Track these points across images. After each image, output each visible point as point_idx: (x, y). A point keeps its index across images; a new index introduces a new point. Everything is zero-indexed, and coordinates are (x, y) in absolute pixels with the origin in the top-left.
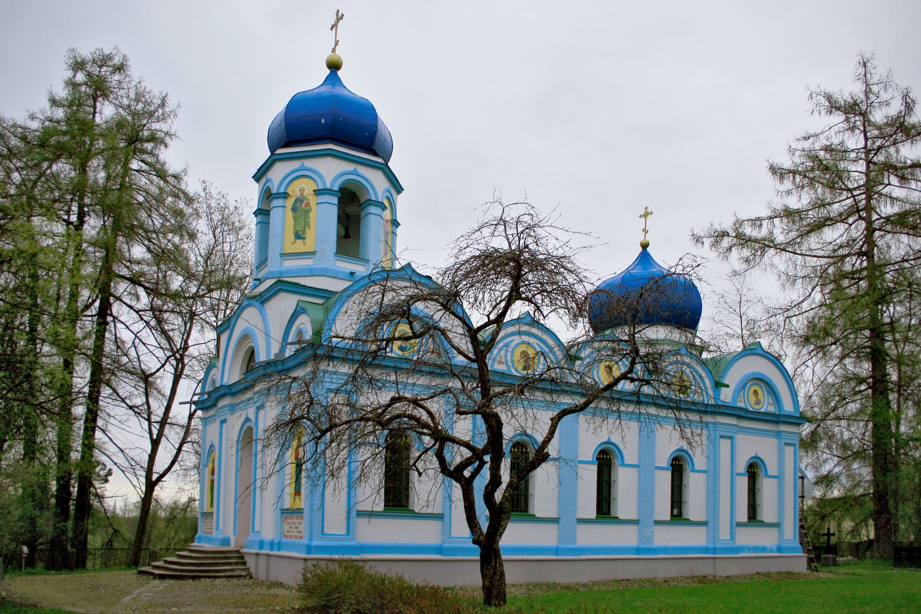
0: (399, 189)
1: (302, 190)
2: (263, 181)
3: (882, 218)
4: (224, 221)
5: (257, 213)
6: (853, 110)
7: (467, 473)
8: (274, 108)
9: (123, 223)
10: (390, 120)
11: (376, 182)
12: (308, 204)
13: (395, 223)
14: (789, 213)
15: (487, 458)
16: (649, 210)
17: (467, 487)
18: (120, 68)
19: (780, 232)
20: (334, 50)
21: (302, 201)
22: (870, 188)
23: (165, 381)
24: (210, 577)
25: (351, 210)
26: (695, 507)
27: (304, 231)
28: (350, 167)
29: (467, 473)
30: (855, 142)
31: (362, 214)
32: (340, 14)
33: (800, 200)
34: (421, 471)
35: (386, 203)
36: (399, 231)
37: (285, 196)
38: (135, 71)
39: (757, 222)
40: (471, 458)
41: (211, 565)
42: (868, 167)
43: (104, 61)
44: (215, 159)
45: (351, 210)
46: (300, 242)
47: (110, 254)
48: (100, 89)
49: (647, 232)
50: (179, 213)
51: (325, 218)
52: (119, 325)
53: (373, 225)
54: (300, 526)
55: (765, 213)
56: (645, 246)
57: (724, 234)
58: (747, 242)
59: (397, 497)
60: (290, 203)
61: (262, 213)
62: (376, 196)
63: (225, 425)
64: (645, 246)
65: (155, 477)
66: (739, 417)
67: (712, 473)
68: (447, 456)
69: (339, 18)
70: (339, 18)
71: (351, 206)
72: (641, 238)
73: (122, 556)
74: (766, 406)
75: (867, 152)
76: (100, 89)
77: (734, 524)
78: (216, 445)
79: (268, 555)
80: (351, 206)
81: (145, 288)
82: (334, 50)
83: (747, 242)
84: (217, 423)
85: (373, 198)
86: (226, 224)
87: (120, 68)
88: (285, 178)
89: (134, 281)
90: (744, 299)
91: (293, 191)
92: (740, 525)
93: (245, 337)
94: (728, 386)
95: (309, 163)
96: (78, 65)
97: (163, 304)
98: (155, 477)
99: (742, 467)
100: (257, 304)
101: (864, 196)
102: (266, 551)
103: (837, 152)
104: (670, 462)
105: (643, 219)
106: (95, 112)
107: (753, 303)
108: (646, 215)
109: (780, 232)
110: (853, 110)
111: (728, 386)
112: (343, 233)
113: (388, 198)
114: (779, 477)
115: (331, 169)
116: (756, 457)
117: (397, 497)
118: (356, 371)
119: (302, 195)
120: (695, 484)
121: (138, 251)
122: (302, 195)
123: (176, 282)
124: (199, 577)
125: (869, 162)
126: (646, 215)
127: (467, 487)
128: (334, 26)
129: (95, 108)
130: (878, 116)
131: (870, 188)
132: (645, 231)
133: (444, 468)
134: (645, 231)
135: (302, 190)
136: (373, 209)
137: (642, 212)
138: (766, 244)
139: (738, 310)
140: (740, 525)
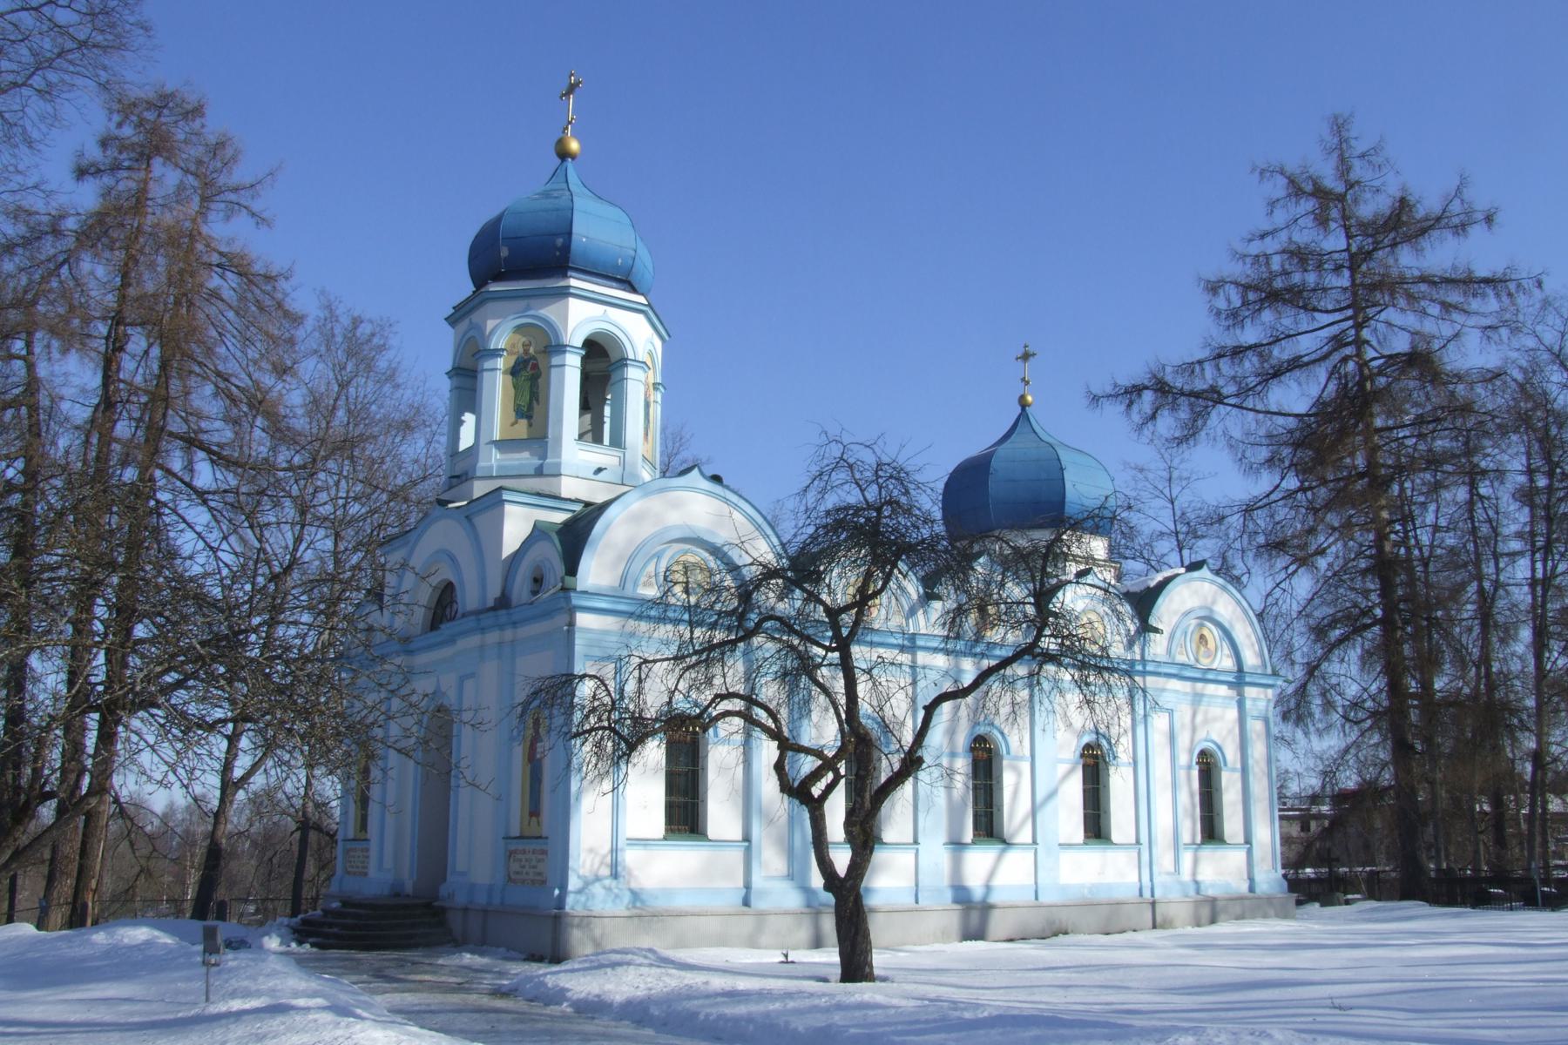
2: (464, 325)
6: (1327, 202)
7: (816, 791)
16: (1030, 350)
17: (816, 807)
18: (197, 111)
28: (599, 309)
29: (816, 791)
31: (614, 377)
38: (214, 125)
39: (1190, 368)
40: (819, 767)
45: (597, 366)
47: (160, 398)
55: (1205, 354)
56: (1023, 404)
57: (1135, 391)
58: (1177, 398)
59: (685, 815)
73: (188, 907)
83: (1177, 398)
87: (197, 111)
90: (1175, 474)
101: (1350, 323)
103: (1300, 256)
104: (1080, 750)
109: (1224, 376)
110: (1327, 202)
118: (132, 324)
120: (1119, 783)
124: (619, 964)
126: (1026, 357)
139: (1166, 491)
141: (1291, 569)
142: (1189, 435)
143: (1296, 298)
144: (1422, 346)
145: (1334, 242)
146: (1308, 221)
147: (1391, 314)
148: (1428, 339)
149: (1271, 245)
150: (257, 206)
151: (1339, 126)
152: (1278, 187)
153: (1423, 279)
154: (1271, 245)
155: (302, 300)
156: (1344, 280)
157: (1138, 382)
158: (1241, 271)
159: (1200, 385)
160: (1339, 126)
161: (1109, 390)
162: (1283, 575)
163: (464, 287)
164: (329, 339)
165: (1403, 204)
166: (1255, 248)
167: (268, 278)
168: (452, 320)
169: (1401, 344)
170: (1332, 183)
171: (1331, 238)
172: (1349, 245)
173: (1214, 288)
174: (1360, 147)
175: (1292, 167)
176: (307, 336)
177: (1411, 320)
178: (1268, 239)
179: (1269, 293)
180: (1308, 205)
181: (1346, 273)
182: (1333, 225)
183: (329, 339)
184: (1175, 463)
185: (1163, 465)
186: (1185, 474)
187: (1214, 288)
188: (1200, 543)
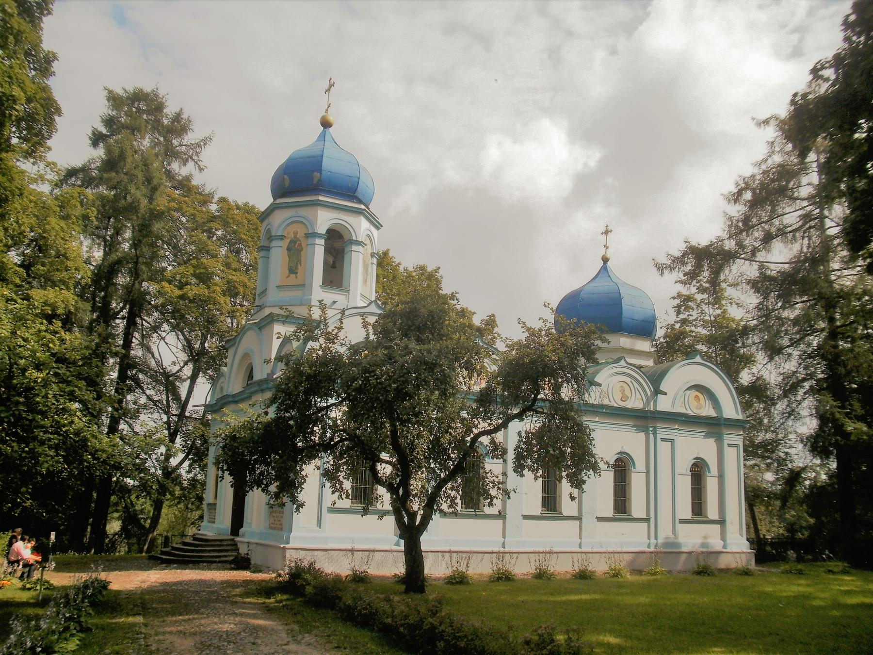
1: (296, 233)
12: (300, 245)
16: (609, 228)
21: (295, 242)
24: (220, 562)
25: (337, 245)
26: (637, 507)
27: (297, 268)
32: (332, 82)
35: (367, 242)
37: (282, 238)
49: (607, 248)
56: (605, 260)
60: (285, 244)
64: (605, 260)
69: (331, 86)
72: (602, 251)
74: (708, 411)
77: (677, 521)
85: (354, 238)
91: (288, 234)
92: (683, 521)
93: (246, 355)
94: (665, 394)
96: (114, 99)
100: (256, 329)
105: (604, 236)
108: (607, 232)
111: (665, 394)
113: (368, 236)
119: (295, 237)
122: (295, 237)
126: (607, 232)
128: (328, 90)
132: (606, 247)
135: (296, 233)
136: (354, 248)
137: (604, 229)
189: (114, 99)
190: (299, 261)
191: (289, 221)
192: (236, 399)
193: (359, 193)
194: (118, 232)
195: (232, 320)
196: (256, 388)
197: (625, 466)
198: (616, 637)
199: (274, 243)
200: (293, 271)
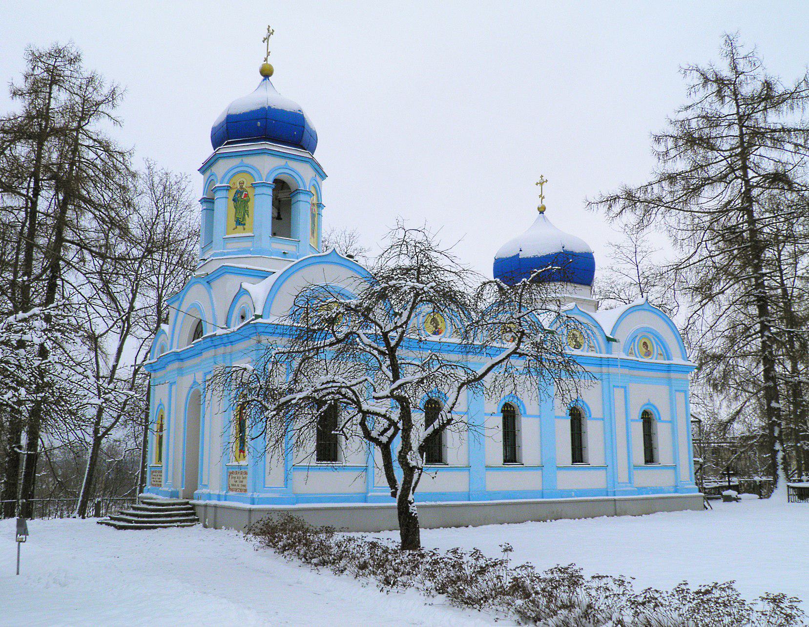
0: (323, 176)
1: (241, 183)
2: (208, 173)
3: (760, 175)
4: (166, 191)
5: (204, 201)
6: (723, 86)
8: (215, 116)
9: (70, 188)
10: (315, 120)
11: (302, 174)
12: (246, 195)
13: (320, 205)
14: (671, 178)
15: (400, 425)
17: (386, 449)
19: (664, 191)
20: (266, 60)
21: (241, 193)
22: (744, 151)
23: (110, 343)
25: (282, 195)
27: (244, 218)
28: (281, 162)
30: (728, 109)
31: (294, 200)
33: (681, 165)
34: (348, 436)
36: (324, 212)
38: (86, 67)
39: (645, 189)
41: (151, 516)
42: (741, 131)
43: (58, 53)
44: (160, 139)
45: (282, 195)
46: (240, 227)
47: (61, 223)
48: (54, 78)
49: (540, 196)
50: (124, 189)
51: (262, 206)
52: (67, 285)
53: (302, 209)
54: (244, 481)
57: (616, 198)
59: (327, 451)
61: (208, 201)
62: (304, 186)
63: (174, 388)
65: (102, 431)
66: (631, 368)
67: (608, 419)
68: (369, 426)
69: (270, 33)
70: (270, 33)
71: (284, 196)
75: (740, 118)
76: (54, 78)
77: (632, 467)
78: (166, 405)
79: (215, 507)
80: (284, 196)
81: (91, 252)
82: (266, 60)
84: (167, 386)
86: (167, 195)
88: (228, 172)
89: (82, 246)
95: (248, 160)
96: (36, 58)
97: (111, 267)
98: (102, 431)
99: (636, 414)
102: (213, 502)
103: (712, 120)
105: (539, 187)
106: (50, 97)
107: (648, 257)
109: (664, 191)
110: (723, 86)
112: (276, 215)
113: (314, 185)
114: (672, 422)
115: (267, 163)
116: (649, 404)
117: (327, 451)
119: (241, 187)
121: (88, 221)
122: (241, 187)
123: (121, 248)
125: (741, 127)
127: (386, 449)
128: (266, 39)
129: (50, 93)
130: (747, 90)
131: (744, 151)
132: (542, 197)
133: (367, 434)
134: (542, 197)
135: (241, 183)
137: (539, 180)
138: (658, 201)
140: (636, 467)
141: (704, 302)
142: (641, 225)
143: (707, 143)
144: (780, 169)
145: (728, 109)
146: (713, 98)
147: (762, 151)
148: (784, 164)
149: (690, 114)
150: (113, 113)
151: (730, 41)
152: (695, 79)
153: (783, 130)
154: (690, 114)
155: (136, 164)
156: (735, 131)
157: (614, 194)
158: (674, 131)
159: (649, 197)
160: (730, 41)
161: (598, 199)
162: (698, 306)
163: (209, 151)
164: (152, 187)
165: (768, 85)
166: (682, 116)
167: (122, 154)
168: (203, 170)
169: (769, 167)
170: (726, 72)
171: (726, 107)
172: (738, 110)
173: (658, 139)
174: (742, 52)
175: (704, 66)
176: (141, 184)
177: (775, 154)
178: (689, 111)
179: (692, 140)
180: (714, 87)
181: (736, 127)
182: (727, 99)
183: (152, 187)
184: (638, 244)
185: (630, 244)
186: (644, 249)
187: (658, 139)
188: (653, 289)
189: (36, 58)
190: (246, 212)
191: (230, 174)
192: (182, 357)
193: (302, 143)
194: (36, 193)
195: (158, 278)
196: (208, 344)
197: (514, 411)
198: (202, 494)
199: (218, 195)
200: (240, 222)
